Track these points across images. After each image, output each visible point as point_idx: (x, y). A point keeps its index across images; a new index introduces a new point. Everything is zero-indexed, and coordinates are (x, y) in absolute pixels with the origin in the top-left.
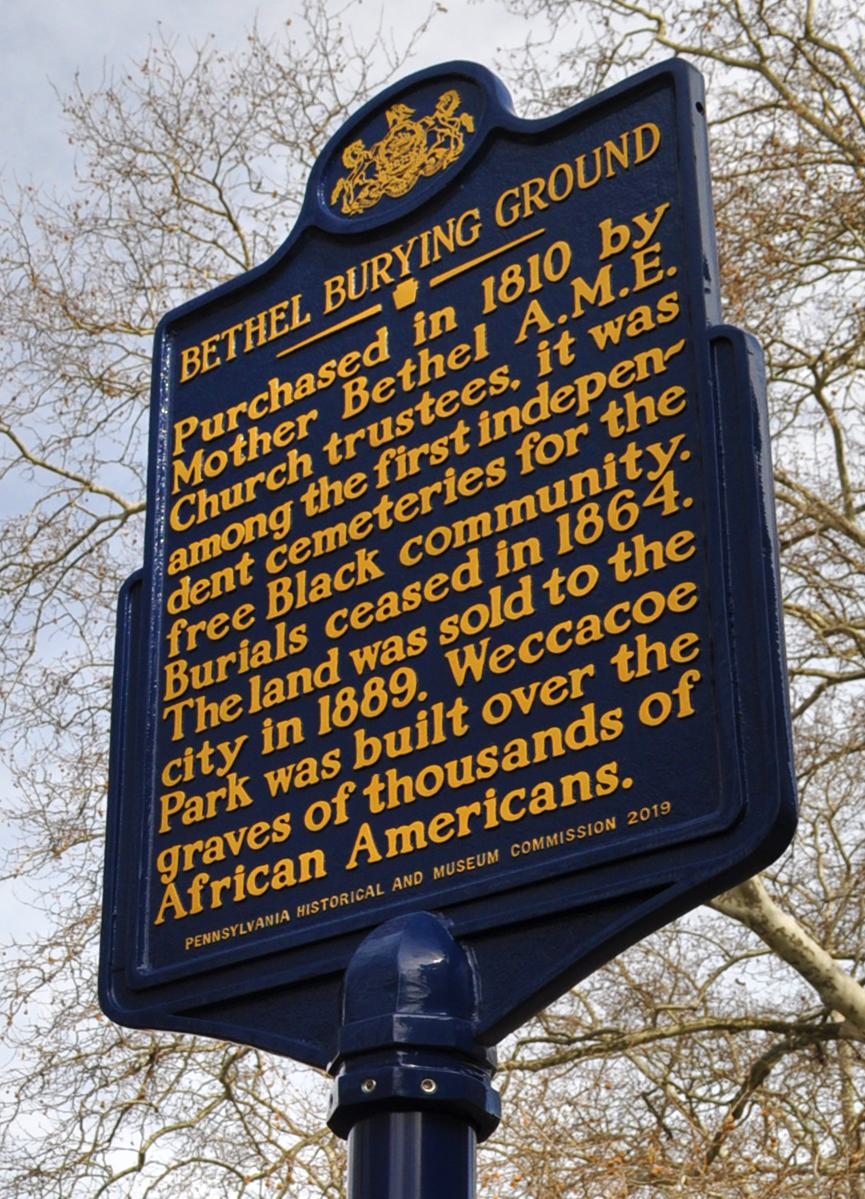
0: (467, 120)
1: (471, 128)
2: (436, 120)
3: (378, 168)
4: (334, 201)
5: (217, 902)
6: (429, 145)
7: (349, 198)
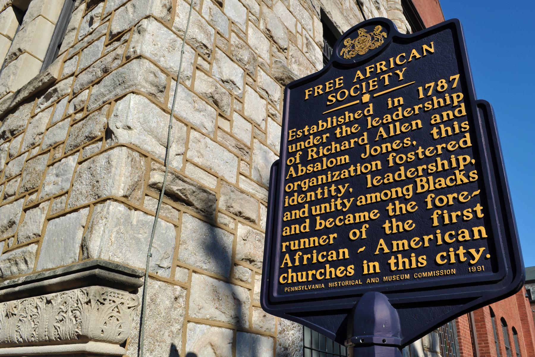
0: (385, 34)
1: (386, 37)
2: (374, 33)
3: (355, 46)
4: (341, 54)
5: (305, 262)
6: (372, 40)
7: (346, 54)
